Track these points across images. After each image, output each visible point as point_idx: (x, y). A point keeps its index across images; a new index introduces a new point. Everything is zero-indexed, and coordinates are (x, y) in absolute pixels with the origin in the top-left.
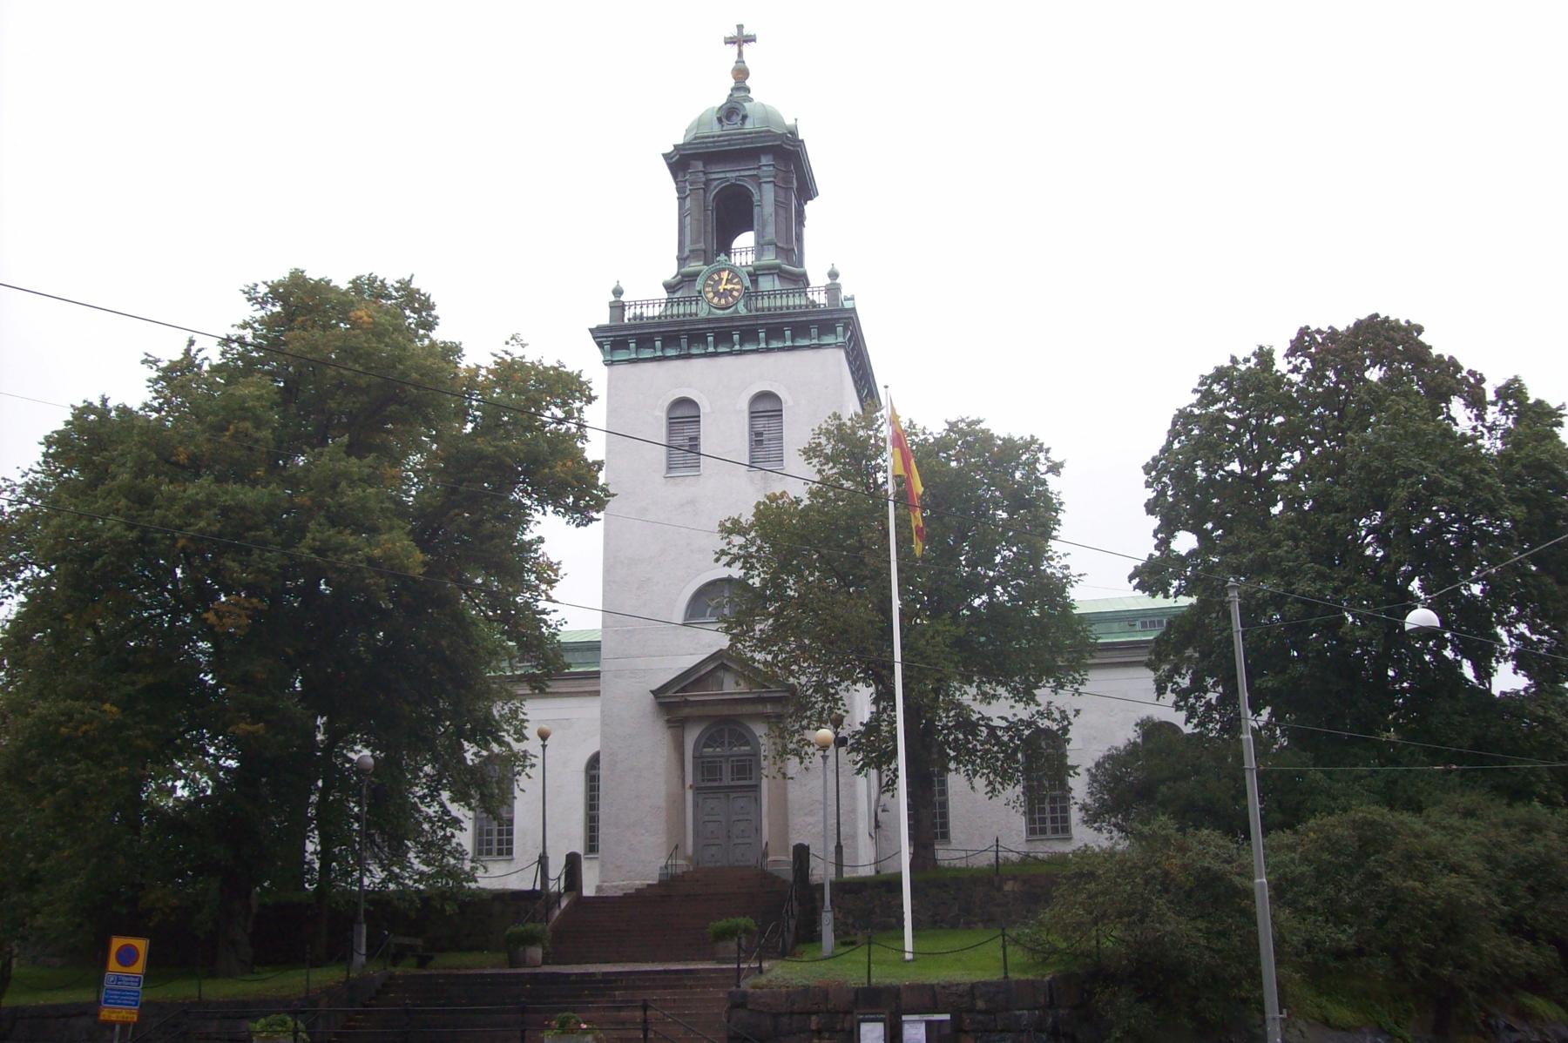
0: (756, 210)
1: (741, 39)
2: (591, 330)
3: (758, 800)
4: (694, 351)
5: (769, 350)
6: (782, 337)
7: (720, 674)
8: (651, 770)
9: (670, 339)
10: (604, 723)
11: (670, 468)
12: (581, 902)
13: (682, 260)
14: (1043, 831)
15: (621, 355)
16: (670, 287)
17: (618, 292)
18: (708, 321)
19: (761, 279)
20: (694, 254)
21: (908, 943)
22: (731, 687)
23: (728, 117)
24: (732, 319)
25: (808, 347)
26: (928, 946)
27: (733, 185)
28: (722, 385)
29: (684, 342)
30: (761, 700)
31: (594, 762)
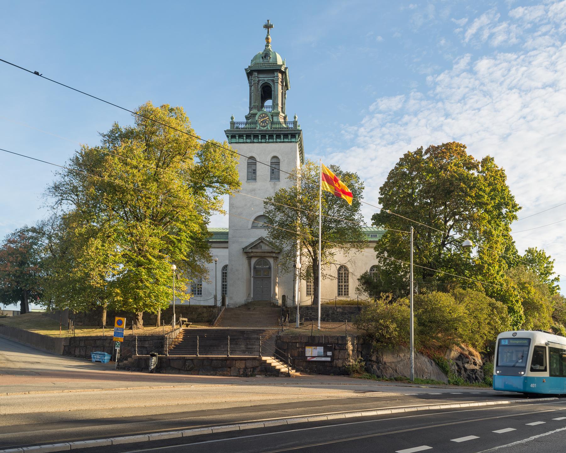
0: (273, 92)
1: (268, 27)
2: (225, 131)
3: (270, 282)
4: (255, 141)
6: (280, 138)
7: (261, 244)
8: (241, 270)
9: (248, 136)
10: (229, 257)
11: (248, 179)
12: (228, 310)
13: (251, 109)
14: (342, 294)
15: (234, 140)
16: (247, 118)
17: (232, 118)
18: (259, 131)
19: (274, 117)
20: (255, 107)
21: (319, 325)
22: (265, 248)
23: (265, 57)
24: (266, 131)
25: (288, 142)
26: (324, 326)
28: (263, 151)
29: (252, 138)
30: (272, 252)
31: (225, 267)
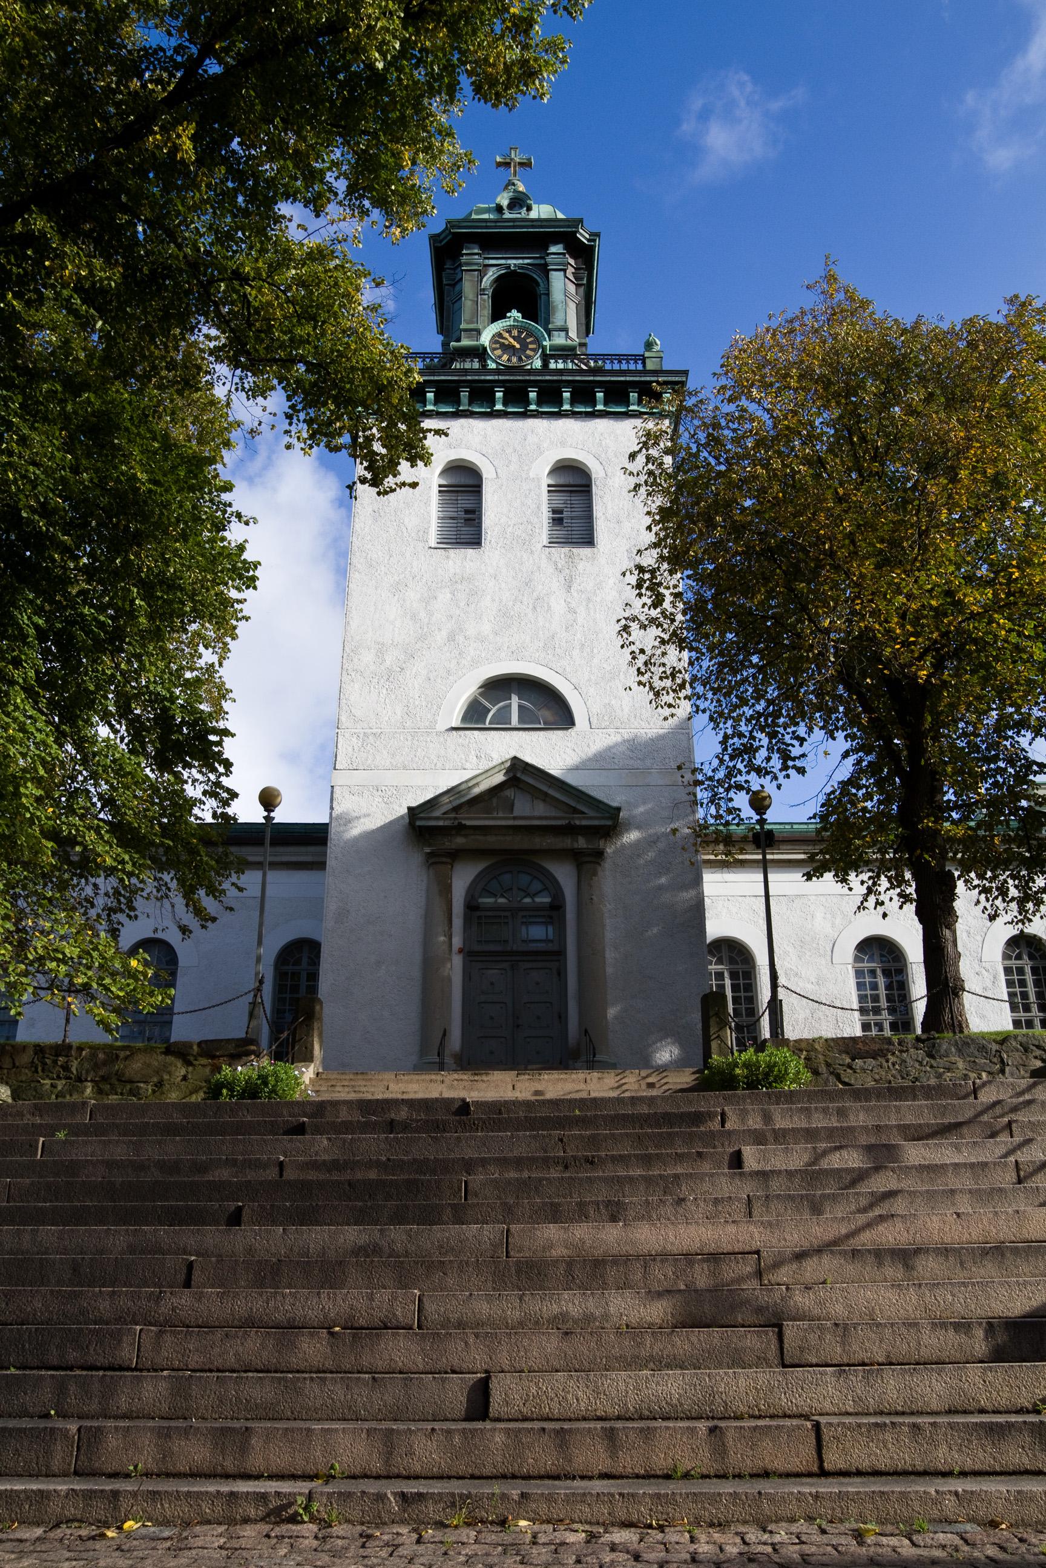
5: (573, 415)
7: (509, 793)
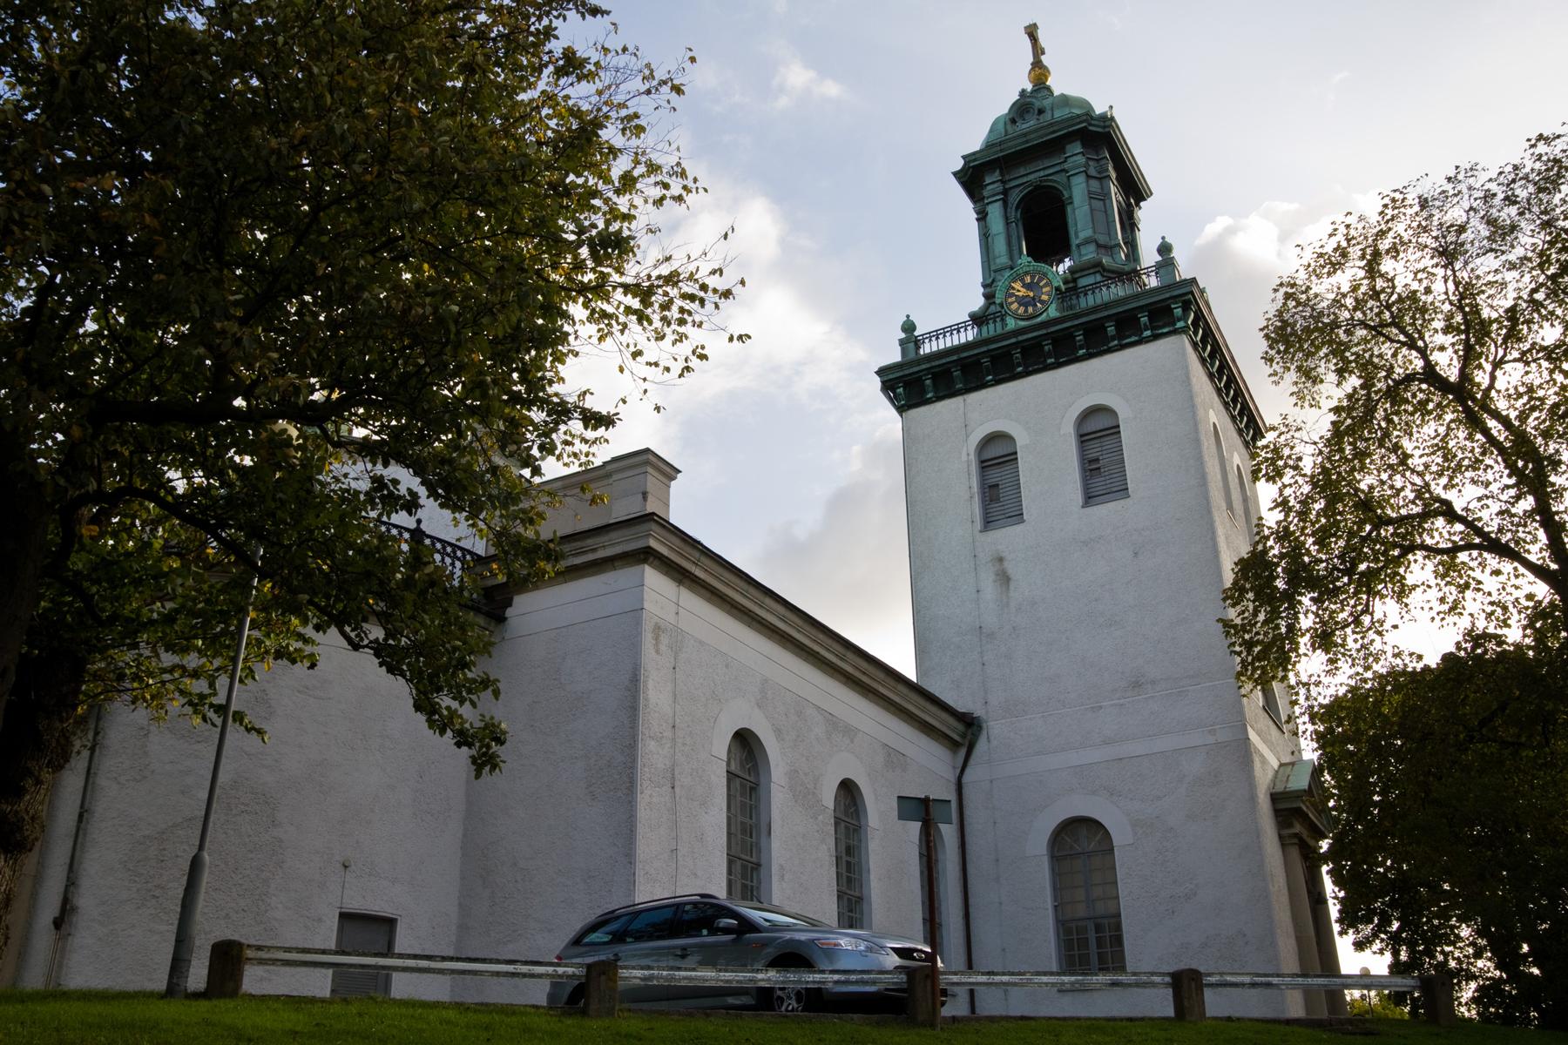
5: (1155, 337)
27: (1037, 188)
